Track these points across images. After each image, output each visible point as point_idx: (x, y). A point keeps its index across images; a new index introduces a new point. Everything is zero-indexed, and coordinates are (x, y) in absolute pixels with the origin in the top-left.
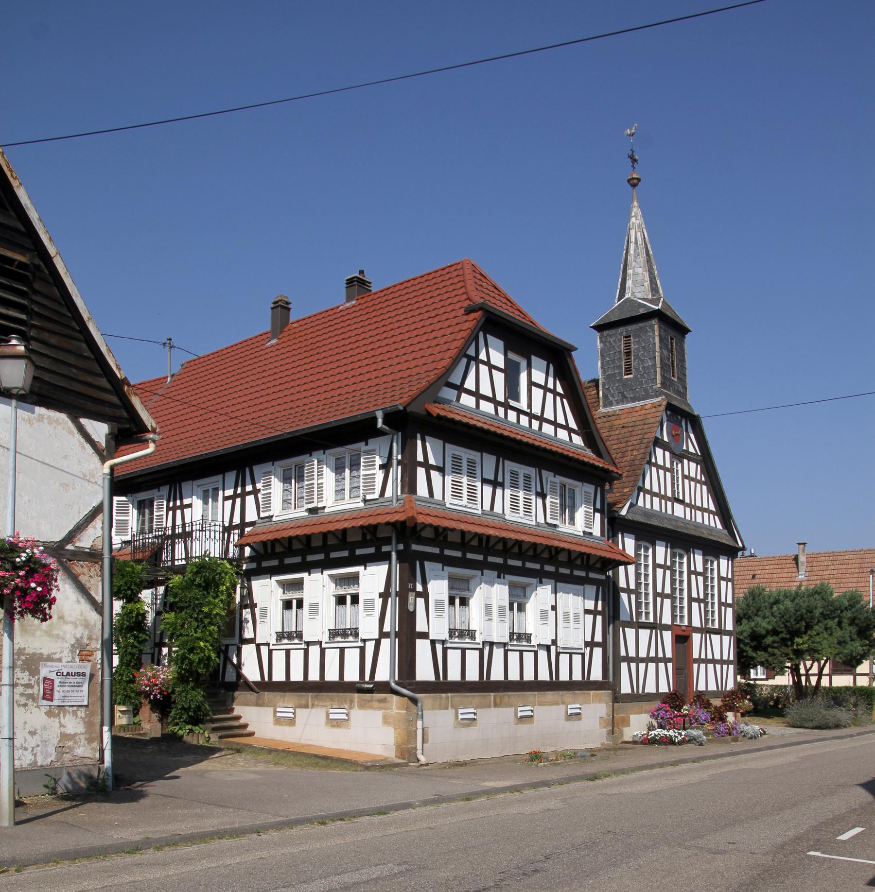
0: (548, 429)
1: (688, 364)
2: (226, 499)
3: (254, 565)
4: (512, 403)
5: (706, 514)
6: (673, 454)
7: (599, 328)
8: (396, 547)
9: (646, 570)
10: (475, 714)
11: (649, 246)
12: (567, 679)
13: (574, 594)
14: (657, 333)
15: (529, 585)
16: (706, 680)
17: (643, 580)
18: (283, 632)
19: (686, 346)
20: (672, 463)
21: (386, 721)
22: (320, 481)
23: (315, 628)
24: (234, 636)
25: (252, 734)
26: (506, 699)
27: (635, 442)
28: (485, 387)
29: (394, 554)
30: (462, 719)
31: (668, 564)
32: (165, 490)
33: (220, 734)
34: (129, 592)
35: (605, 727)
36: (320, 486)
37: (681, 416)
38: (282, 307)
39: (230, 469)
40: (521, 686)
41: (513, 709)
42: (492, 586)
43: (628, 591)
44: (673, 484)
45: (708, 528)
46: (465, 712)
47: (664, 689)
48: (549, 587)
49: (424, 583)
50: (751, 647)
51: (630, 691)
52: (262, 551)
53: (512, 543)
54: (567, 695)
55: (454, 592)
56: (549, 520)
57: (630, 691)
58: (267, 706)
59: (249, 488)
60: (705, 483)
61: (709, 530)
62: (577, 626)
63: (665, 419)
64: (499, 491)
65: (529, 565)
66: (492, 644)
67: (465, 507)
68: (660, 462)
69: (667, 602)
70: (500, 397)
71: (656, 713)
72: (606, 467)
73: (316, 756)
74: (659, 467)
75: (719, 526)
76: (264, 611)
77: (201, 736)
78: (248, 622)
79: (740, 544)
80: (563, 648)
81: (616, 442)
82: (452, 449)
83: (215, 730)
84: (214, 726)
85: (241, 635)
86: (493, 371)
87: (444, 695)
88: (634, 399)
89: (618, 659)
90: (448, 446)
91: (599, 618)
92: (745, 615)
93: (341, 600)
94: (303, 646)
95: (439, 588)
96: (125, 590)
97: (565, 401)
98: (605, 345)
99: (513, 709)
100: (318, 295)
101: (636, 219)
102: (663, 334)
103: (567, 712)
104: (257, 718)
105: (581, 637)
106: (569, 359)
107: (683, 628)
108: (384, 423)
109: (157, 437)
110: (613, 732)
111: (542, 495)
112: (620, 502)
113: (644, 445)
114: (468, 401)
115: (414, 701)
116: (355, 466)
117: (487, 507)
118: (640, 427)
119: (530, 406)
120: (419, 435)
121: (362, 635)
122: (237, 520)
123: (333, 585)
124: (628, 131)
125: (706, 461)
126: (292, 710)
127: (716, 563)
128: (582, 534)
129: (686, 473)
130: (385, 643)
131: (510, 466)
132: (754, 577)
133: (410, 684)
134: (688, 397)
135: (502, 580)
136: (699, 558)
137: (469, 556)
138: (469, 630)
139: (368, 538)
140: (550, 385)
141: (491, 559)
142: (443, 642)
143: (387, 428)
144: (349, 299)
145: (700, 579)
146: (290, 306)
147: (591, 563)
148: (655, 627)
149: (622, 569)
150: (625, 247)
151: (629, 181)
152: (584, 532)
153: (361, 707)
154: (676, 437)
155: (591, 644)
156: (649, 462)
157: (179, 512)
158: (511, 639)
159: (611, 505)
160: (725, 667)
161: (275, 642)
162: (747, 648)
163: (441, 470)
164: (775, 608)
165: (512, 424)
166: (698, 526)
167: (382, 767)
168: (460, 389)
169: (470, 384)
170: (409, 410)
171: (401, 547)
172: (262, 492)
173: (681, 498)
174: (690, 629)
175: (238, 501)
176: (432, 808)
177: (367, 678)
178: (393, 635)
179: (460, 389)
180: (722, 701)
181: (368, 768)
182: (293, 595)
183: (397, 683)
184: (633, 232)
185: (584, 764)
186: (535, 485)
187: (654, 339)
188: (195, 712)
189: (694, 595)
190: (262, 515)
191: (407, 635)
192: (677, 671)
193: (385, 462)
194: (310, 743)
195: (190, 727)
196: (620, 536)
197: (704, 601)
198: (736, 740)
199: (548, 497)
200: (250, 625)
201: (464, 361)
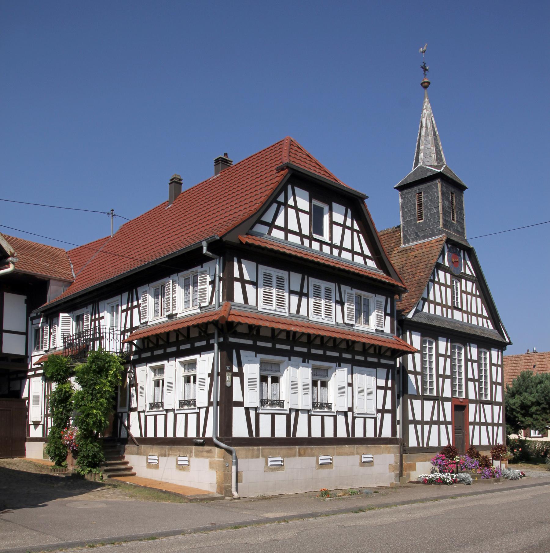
0: (346, 256)
1: (465, 212)
2: (123, 311)
3: (137, 357)
4: (315, 236)
5: (480, 319)
6: (453, 275)
7: (400, 188)
8: (218, 340)
9: (428, 359)
10: (282, 461)
11: (436, 129)
12: (153, 436)
13: (367, 375)
14: (440, 189)
15: (330, 368)
16: (479, 437)
17: (483, 374)
18: (154, 403)
19: (464, 199)
20: (452, 282)
21: (211, 466)
22: (174, 296)
23: (171, 401)
24: (126, 406)
25: (134, 474)
26: (309, 451)
27: (423, 267)
28: (291, 224)
29: (216, 346)
30: (271, 465)
31: (449, 353)
32: (90, 307)
33: (109, 474)
34: (59, 377)
35: (393, 471)
36: (174, 299)
37: (459, 248)
38: (176, 182)
39: (124, 291)
40: (323, 441)
41: (315, 458)
42: (298, 368)
43: (415, 373)
44: (453, 297)
45: (482, 329)
46: (274, 460)
47: (444, 443)
48: (346, 369)
49: (240, 366)
50: (521, 414)
51: (416, 445)
52: (141, 347)
53: (340, 340)
54: (361, 448)
55: (316, 378)
56: (346, 321)
57: (416, 445)
58: (143, 455)
59: (135, 303)
60: (479, 297)
61: (482, 330)
62: (370, 398)
63: (446, 250)
64: (304, 300)
65: (329, 353)
66: (297, 411)
67: (275, 310)
68: (442, 281)
69: (448, 382)
70: (306, 231)
71: (435, 461)
72: (392, 282)
73: (161, 491)
74: (441, 284)
75: (491, 327)
76: (142, 387)
77: (97, 475)
78: (134, 396)
79: (507, 340)
80: (358, 414)
81: (410, 267)
82: (263, 269)
83: (106, 471)
84: (106, 468)
85: (130, 405)
86: (300, 213)
87: (256, 448)
88: (424, 237)
89: (406, 423)
90: (260, 266)
91: (389, 393)
92: (517, 391)
93: (187, 380)
94: (164, 413)
95: (252, 370)
96: (57, 375)
97: (361, 235)
98: (404, 200)
99: (315, 458)
100: (198, 173)
101: (427, 110)
102: (445, 190)
103: (361, 460)
104: (137, 461)
105: (374, 406)
106: (362, 205)
107: (461, 400)
108: (208, 250)
109: (14, 260)
110: (401, 474)
111: (341, 303)
112: (408, 309)
113: (428, 269)
114: (278, 234)
115: (230, 452)
116: (195, 284)
117: (294, 310)
118: (427, 256)
119: (331, 238)
120: (235, 259)
121: (198, 404)
122: (128, 326)
123: (183, 369)
124: (421, 50)
125: (479, 280)
126: (156, 458)
127: (488, 354)
128: (374, 331)
129: (464, 289)
130: (211, 408)
131: (313, 281)
132: (534, 366)
133: (229, 439)
134: (465, 235)
135: (306, 364)
136: (474, 351)
137: (278, 346)
138: (279, 401)
139: (202, 334)
140: (348, 223)
141: (296, 349)
142: (256, 409)
143: (210, 254)
144: (216, 174)
145: (475, 365)
146: (182, 182)
147: (382, 351)
148: (438, 399)
149: (410, 356)
150: (419, 131)
151: (422, 84)
152: (376, 330)
153: (197, 456)
154: (455, 263)
155: (382, 411)
156: (433, 281)
157: (97, 322)
158: (314, 407)
159: (400, 312)
160: (495, 428)
161: (149, 410)
162: (519, 415)
163: (255, 284)
164: (539, 386)
165: (316, 251)
166: (472, 327)
167: (202, 500)
168: (272, 225)
169: (280, 222)
170: (224, 239)
171: (221, 340)
172: (142, 305)
173: (460, 307)
174: (468, 400)
175: (129, 312)
176: (200, 534)
177: (201, 436)
178: (215, 404)
179: (272, 225)
180: (492, 452)
181: (191, 501)
182: (159, 377)
183: (218, 439)
184: (424, 120)
185: (361, 499)
186: (334, 295)
187: (438, 193)
188: (93, 459)
189: (470, 376)
190: (142, 321)
191: (226, 403)
192: (455, 431)
193: (213, 279)
194: (167, 481)
195: (89, 469)
196: (408, 333)
197: (479, 381)
198: (498, 481)
199: (346, 305)
200: (135, 398)
201: (275, 206)
